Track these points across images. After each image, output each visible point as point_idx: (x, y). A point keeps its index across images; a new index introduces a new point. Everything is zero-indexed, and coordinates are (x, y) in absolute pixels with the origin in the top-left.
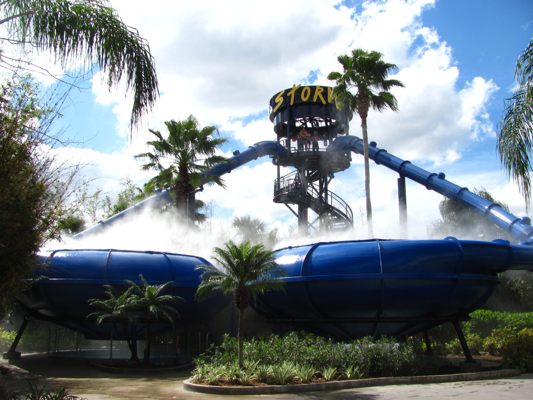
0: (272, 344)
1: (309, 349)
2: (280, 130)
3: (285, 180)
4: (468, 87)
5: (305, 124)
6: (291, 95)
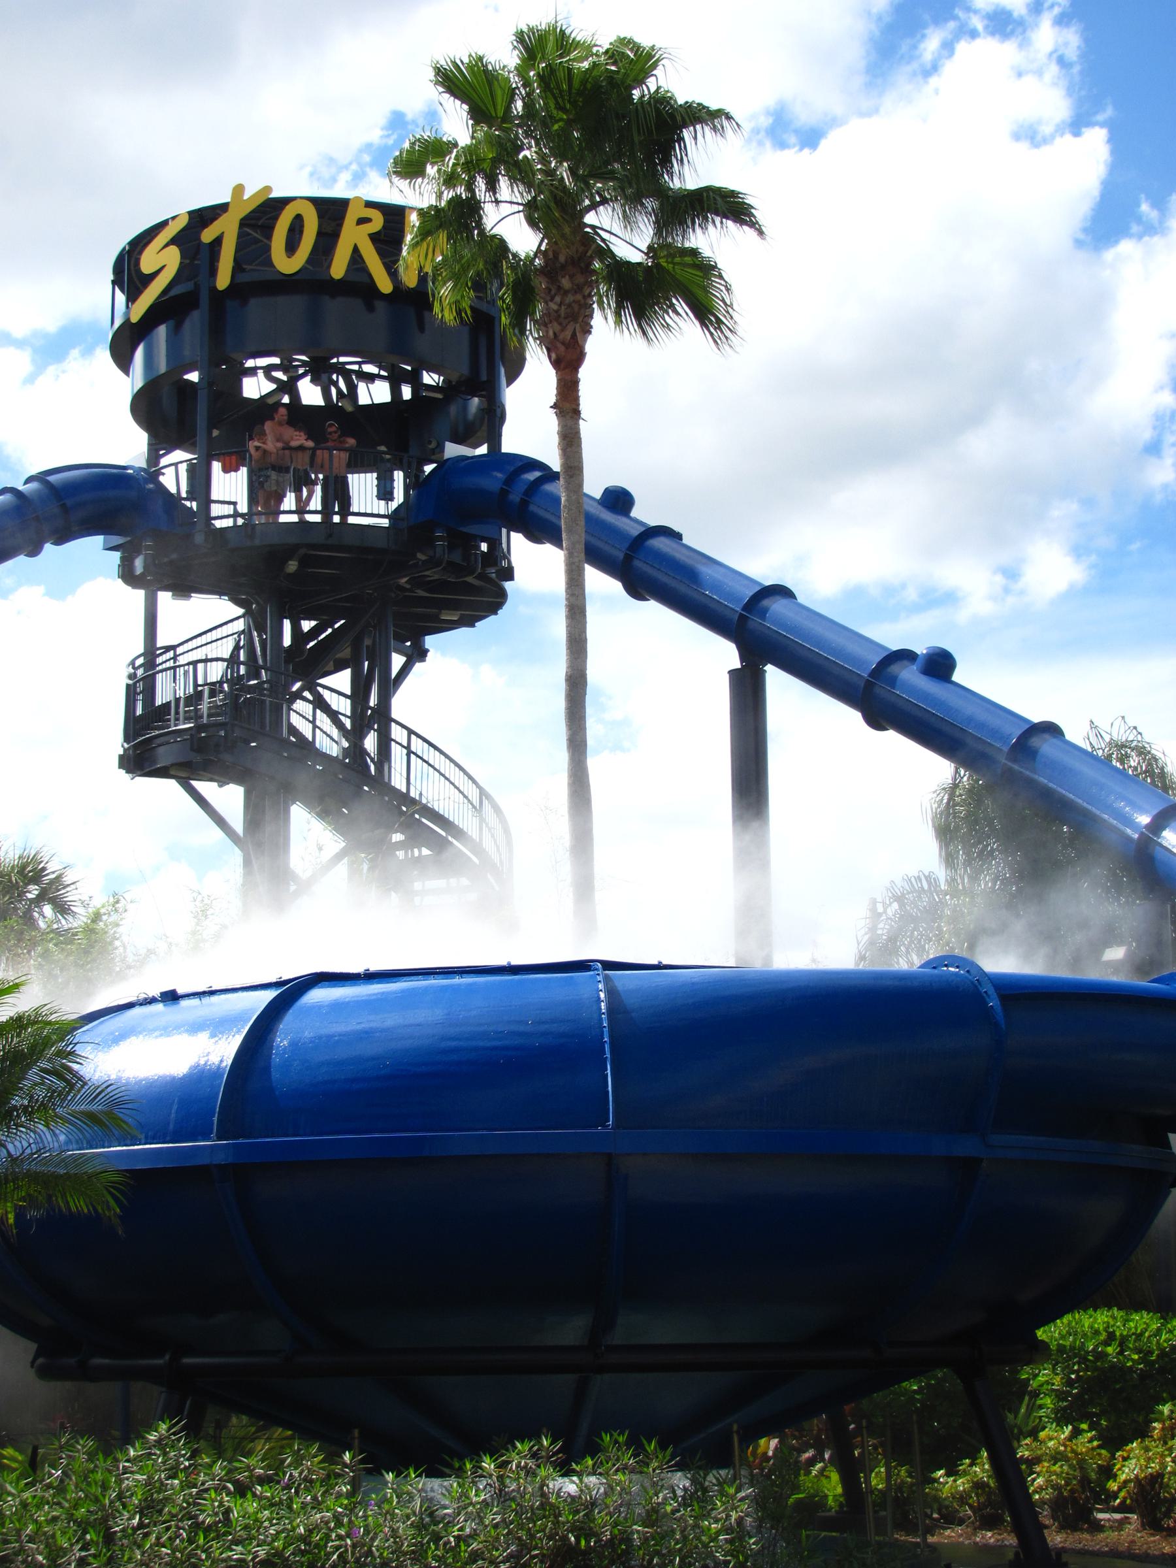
0: (61, 1489)
1: (242, 1509)
2: (161, 412)
3: (182, 660)
4: (1150, 230)
5: (289, 387)
6: (218, 241)
